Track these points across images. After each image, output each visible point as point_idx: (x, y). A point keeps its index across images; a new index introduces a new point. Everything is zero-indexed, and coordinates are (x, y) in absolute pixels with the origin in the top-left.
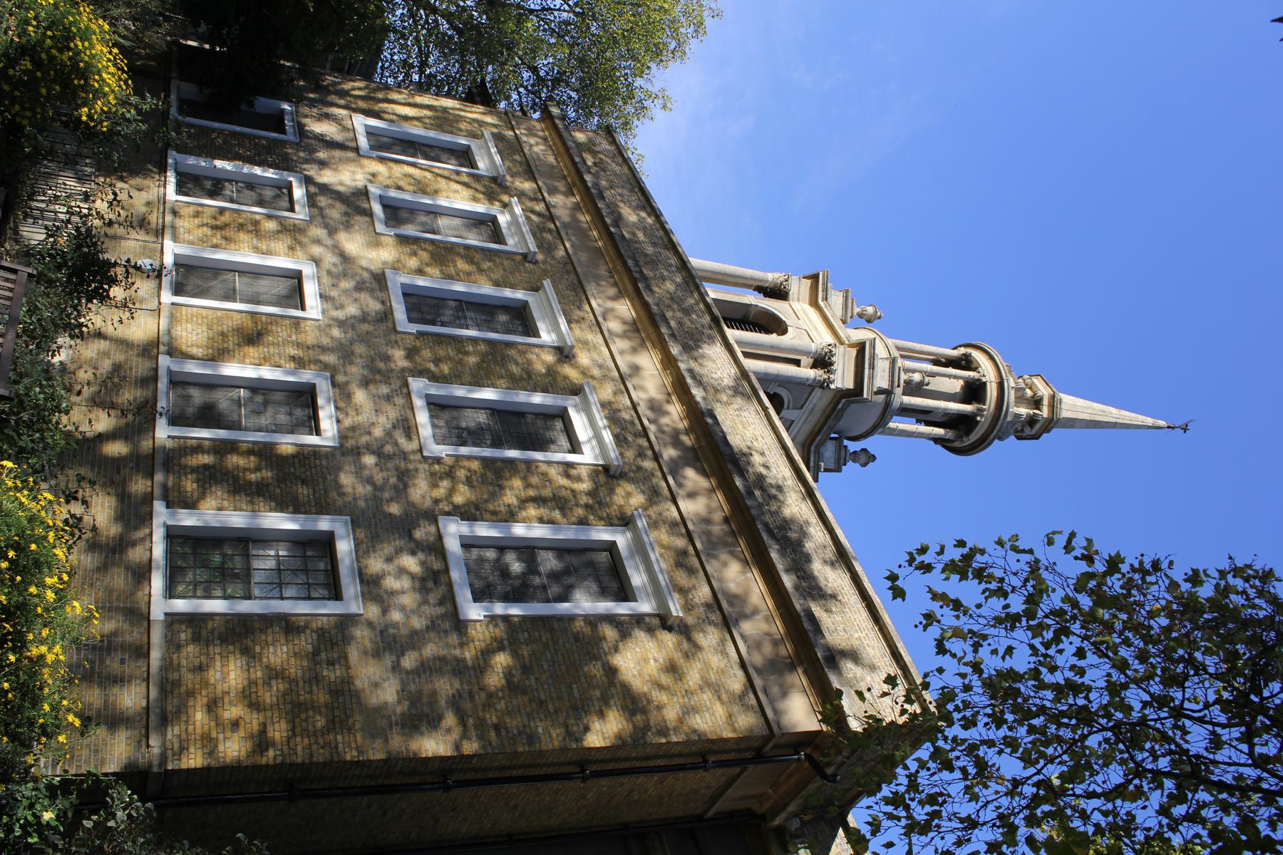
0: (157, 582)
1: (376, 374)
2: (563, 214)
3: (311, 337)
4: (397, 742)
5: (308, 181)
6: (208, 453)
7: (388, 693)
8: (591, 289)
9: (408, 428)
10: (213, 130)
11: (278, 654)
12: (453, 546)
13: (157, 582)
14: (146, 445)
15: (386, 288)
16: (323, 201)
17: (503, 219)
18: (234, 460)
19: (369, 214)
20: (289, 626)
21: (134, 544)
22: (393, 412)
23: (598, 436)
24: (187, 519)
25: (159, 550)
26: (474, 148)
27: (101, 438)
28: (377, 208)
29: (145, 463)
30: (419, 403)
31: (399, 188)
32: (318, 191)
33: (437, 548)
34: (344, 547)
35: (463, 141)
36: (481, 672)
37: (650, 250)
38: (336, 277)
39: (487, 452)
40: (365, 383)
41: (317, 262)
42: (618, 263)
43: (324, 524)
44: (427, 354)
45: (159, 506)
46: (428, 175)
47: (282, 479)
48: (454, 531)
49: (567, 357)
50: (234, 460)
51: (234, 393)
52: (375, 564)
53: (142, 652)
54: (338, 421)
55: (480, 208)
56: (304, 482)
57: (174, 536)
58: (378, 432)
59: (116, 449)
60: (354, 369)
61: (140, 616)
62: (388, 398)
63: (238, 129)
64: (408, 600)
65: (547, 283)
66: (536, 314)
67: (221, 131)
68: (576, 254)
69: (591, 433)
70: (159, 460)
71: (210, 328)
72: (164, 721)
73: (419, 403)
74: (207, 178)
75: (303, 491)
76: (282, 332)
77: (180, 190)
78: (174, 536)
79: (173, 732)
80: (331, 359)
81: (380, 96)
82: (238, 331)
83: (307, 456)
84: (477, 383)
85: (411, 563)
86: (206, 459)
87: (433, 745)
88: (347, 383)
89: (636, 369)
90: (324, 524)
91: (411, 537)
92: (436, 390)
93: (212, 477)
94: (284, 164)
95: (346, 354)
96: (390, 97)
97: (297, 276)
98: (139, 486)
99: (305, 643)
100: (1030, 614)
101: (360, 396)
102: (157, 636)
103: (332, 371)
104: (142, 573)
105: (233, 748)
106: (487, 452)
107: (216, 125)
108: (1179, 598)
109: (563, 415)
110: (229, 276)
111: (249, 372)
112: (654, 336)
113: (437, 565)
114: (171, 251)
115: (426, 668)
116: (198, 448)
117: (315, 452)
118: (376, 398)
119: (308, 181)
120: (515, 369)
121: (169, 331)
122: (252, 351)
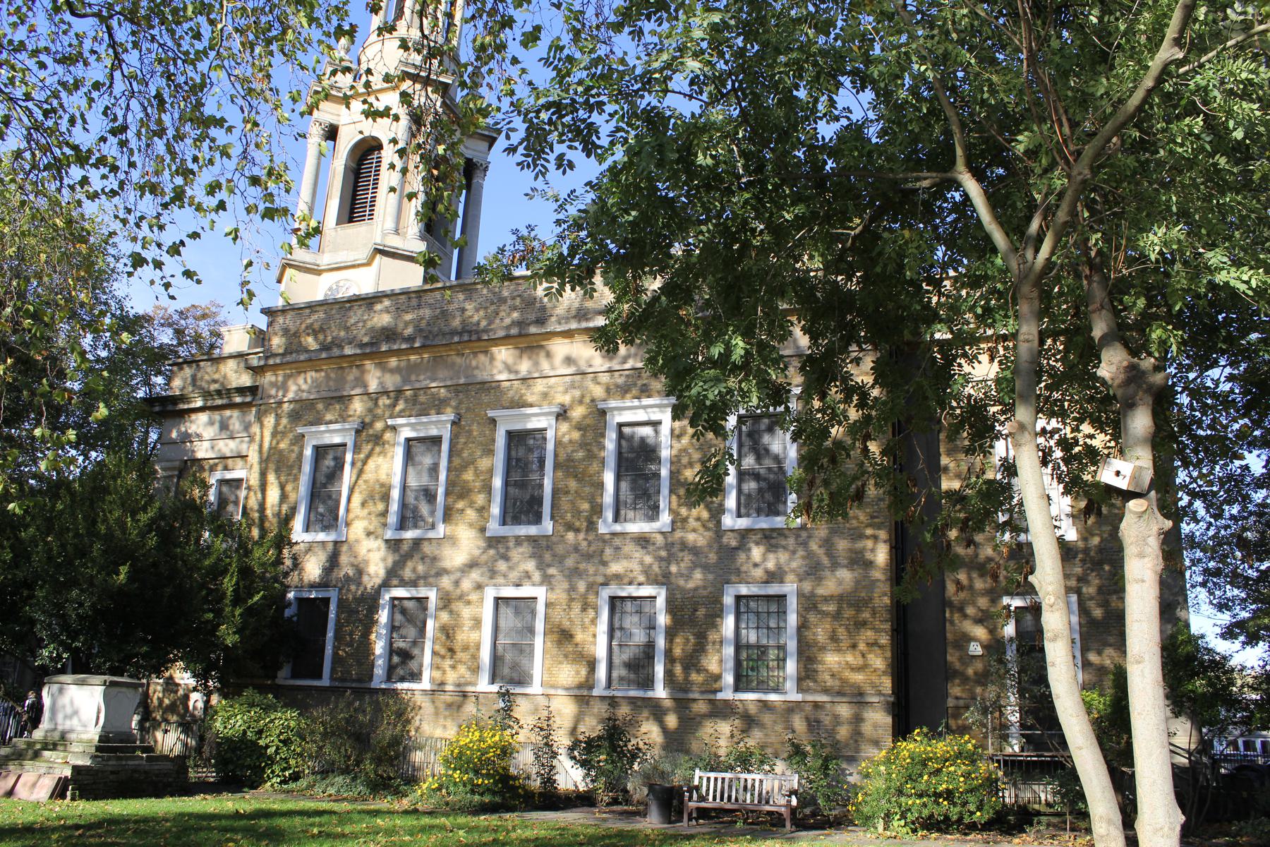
0: (773, 697)
1: (596, 556)
3: (560, 595)
4: (877, 575)
5: (386, 584)
7: (845, 575)
8: (482, 376)
9: (643, 541)
10: (335, 654)
11: (820, 634)
13: (773, 697)
16: (407, 573)
17: (407, 433)
18: (678, 651)
19: (417, 543)
20: (802, 627)
21: (746, 711)
22: (629, 548)
24: (729, 679)
26: (315, 443)
28: (410, 534)
29: (682, 704)
31: (384, 514)
32: (393, 576)
33: (744, 534)
34: (744, 590)
35: (308, 452)
36: (1172, 751)
37: (426, 313)
38: (493, 573)
39: (665, 491)
40: (605, 564)
42: (453, 347)
43: (728, 600)
45: (720, 696)
47: (692, 622)
49: (565, 412)
50: (678, 651)
53: (816, 705)
54: (640, 584)
55: (399, 452)
56: (696, 610)
59: (672, 721)
60: (591, 570)
62: (618, 548)
63: (330, 634)
66: (518, 427)
67: (336, 649)
69: (641, 411)
70: (681, 695)
71: (561, 663)
72: (861, 694)
73: (618, 528)
74: (390, 659)
75: (701, 612)
78: (737, 689)
79: (869, 690)
80: (582, 586)
83: (671, 607)
84: (600, 485)
85: (757, 552)
87: (881, 555)
90: (728, 600)
91: (736, 549)
92: (609, 515)
93: (692, 661)
94: (371, 602)
95: (574, 573)
96: (256, 507)
98: (701, 707)
99: (812, 618)
101: (615, 568)
102: (810, 698)
103: (593, 588)
104: (765, 705)
105: (878, 662)
106: (665, 491)
108: (986, 141)
109: (620, 425)
110: (500, 648)
111: (602, 640)
112: (538, 338)
114: (483, 685)
115: (830, 554)
119: (386, 584)
120: (580, 454)
121: (567, 689)
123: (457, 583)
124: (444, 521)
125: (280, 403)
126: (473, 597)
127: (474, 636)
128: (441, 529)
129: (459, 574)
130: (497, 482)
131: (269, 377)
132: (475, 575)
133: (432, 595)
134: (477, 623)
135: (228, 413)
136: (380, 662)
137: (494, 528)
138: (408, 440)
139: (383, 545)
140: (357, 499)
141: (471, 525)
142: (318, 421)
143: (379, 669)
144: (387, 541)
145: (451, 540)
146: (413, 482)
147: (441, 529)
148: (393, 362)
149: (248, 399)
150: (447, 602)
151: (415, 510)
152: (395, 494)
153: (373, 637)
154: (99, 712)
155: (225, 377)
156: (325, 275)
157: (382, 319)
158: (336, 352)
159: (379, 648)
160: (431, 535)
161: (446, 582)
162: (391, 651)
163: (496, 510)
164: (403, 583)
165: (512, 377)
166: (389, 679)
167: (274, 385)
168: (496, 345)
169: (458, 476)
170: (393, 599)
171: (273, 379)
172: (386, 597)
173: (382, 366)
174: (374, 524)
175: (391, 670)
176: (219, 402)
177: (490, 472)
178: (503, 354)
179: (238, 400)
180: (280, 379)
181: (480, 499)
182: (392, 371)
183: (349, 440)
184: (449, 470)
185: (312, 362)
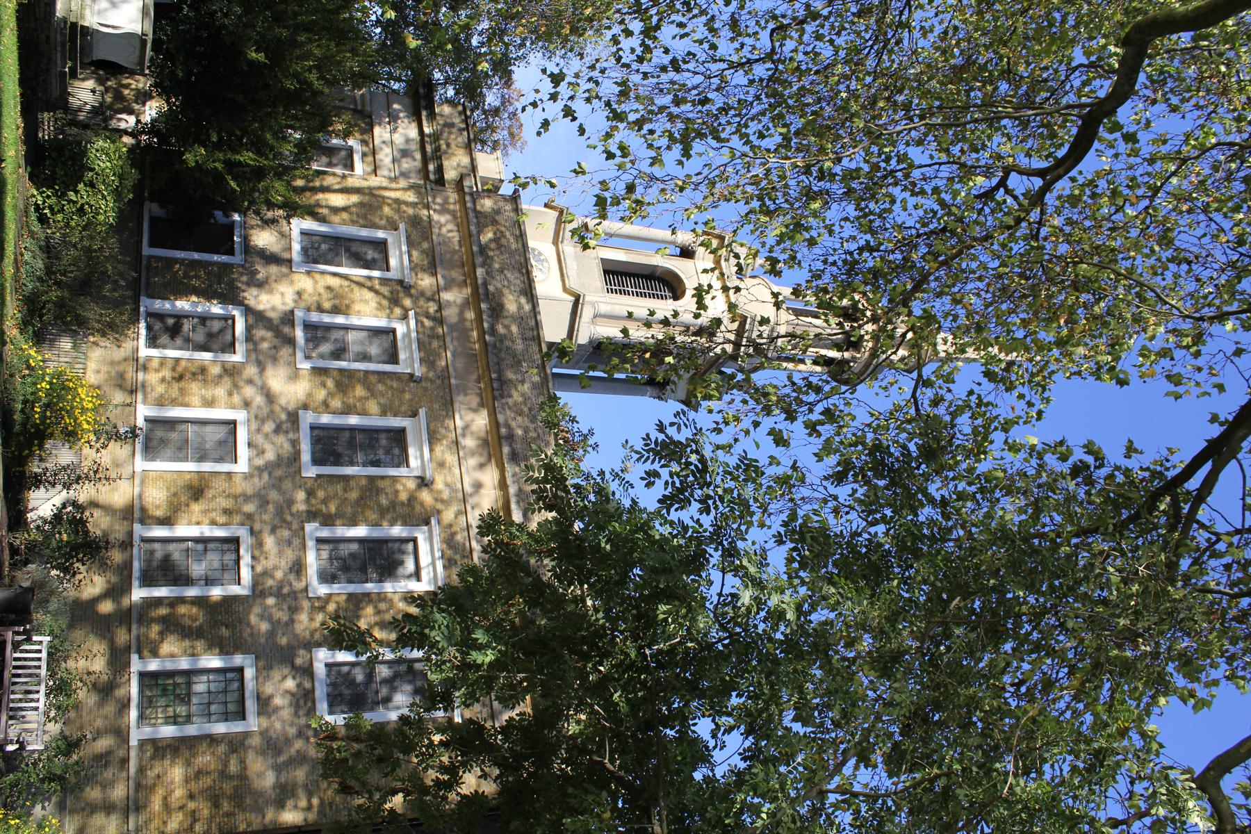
2: (451, 314)
3: (240, 486)
4: (270, 815)
5: (248, 311)
6: (280, 208)
8: (459, 399)
10: (176, 261)
11: (205, 759)
12: (320, 669)
13: (134, 713)
14: (125, 602)
15: (298, 429)
16: (260, 333)
17: (400, 329)
18: (182, 610)
19: (291, 341)
20: (212, 740)
22: (290, 555)
23: (433, 564)
24: (153, 665)
25: (134, 689)
26: (390, 240)
27: (96, 600)
28: (299, 334)
29: (125, 617)
30: (311, 544)
31: (320, 309)
32: (256, 318)
33: (308, 671)
34: (249, 673)
35: (381, 234)
38: (261, 420)
41: (247, 404)
43: (238, 660)
44: (321, 494)
46: (346, 283)
48: (322, 656)
50: (182, 610)
51: (184, 545)
52: (268, 689)
53: (125, 761)
54: (253, 567)
57: (142, 675)
58: (279, 575)
59: (106, 607)
60: (266, 517)
61: (122, 735)
62: (289, 543)
63: (196, 256)
64: (286, 714)
65: (422, 412)
68: (453, 361)
70: (134, 615)
74: (170, 316)
75: (224, 632)
76: (219, 485)
77: (153, 341)
78: (142, 675)
80: (249, 508)
81: (317, 184)
82: (189, 487)
83: (228, 601)
84: (353, 523)
85: (290, 684)
86: (163, 611)
88: (261, 532)
89: (478, 486)
90: (238, 660)
92: (325, 533)
97: (234, 423)
98: (122, 637)
100: (1040, 457)
101: (269, 542)
102: (133, 754)
104: (125, 705)
107: (180, 254)
110: (183, 427)
111: (193, 531)
113: (307, 685)
116: (158, 602)
117: (235, 598)
118: (279, 542)
119: (248, 311)
120: (384, 501)
122: (196, 507)
123: (250, 382)
124: (313, 368)
125: (428, 207)
126: (236, 399)
127: (196, 400)
128: (305, 366)
129: (259, 383)
130: (353, 420)
131: (453, 196)
132: (259, 400)
133: (238, 357)
134: (209, 403)
135: (418, 156)
136: (168, 305)
137: (308, 418)
138: (394, 331)
139: (288, 308)
140: (335, 282)
141: (309, 395)
142: (410, 244)
143: (159, 305)
144: (292, 312)
145: (295, 375)
146: (351, 336)
147: (305, 366)
148: (470, 315)
149: (432, 177)
150: (231, 372)
151: (325, 339)
152: (340, 320)
153: (194, 298)
154: (113, 27)
155: (454, 154)
156: (553, 248)
157: (512, 304)
158: (479, 260)
159: (183, 305)
160: (299, 355)
161: (251, 371)
162: (180, 317)
163: (326, 419)
164: (249, 329)
165: (459, 431)
166: (150, 314)
167: (446, 201)
168: (489, 415)
169: (359, 381)
170: (233, 318)
171: (451, 200)
172: (236, 313)
173: (466, 304)
174: (309, 299)
175: (160, 316)
176: (429, 149)
177: (364, 413)
178: (481, 421)
179: (431, 167)
180: (452, 207)
181: (336, 403)
182: (461, 313)
183: (393, 274)
184: (366, 372)
185: (468, 238)
